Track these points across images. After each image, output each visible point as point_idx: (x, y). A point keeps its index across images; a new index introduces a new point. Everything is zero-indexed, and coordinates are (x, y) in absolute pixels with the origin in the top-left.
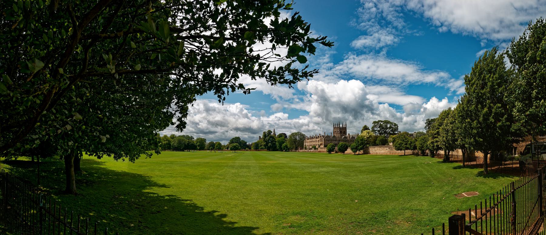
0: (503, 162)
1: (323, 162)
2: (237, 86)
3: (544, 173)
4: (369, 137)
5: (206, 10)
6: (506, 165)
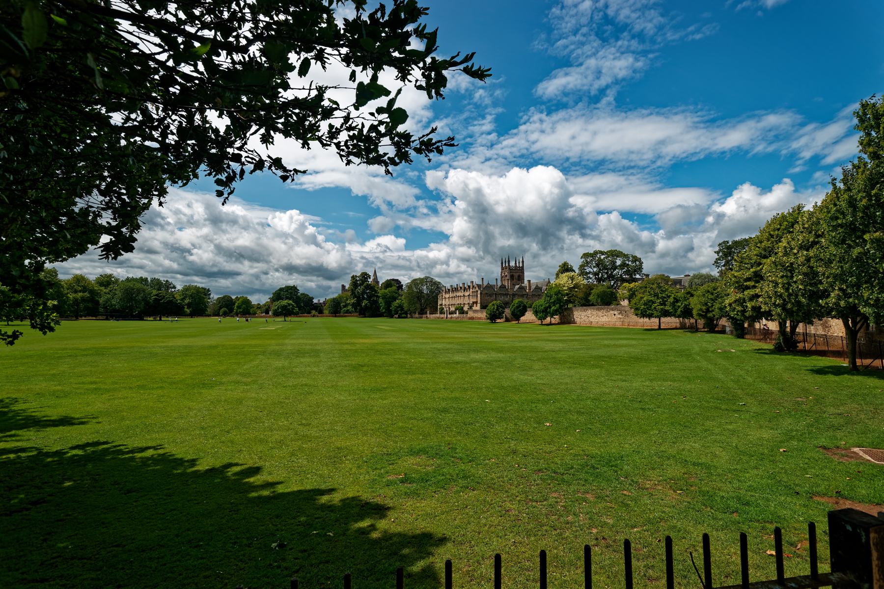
4: (574, 288)
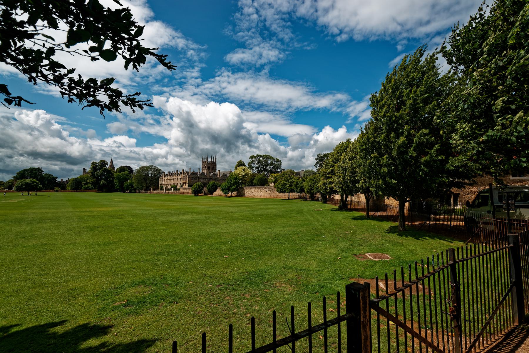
0: (432, 216)
1: (186, 207)
3: (525, 243)
4: (245, 175)
6: (438, 220)
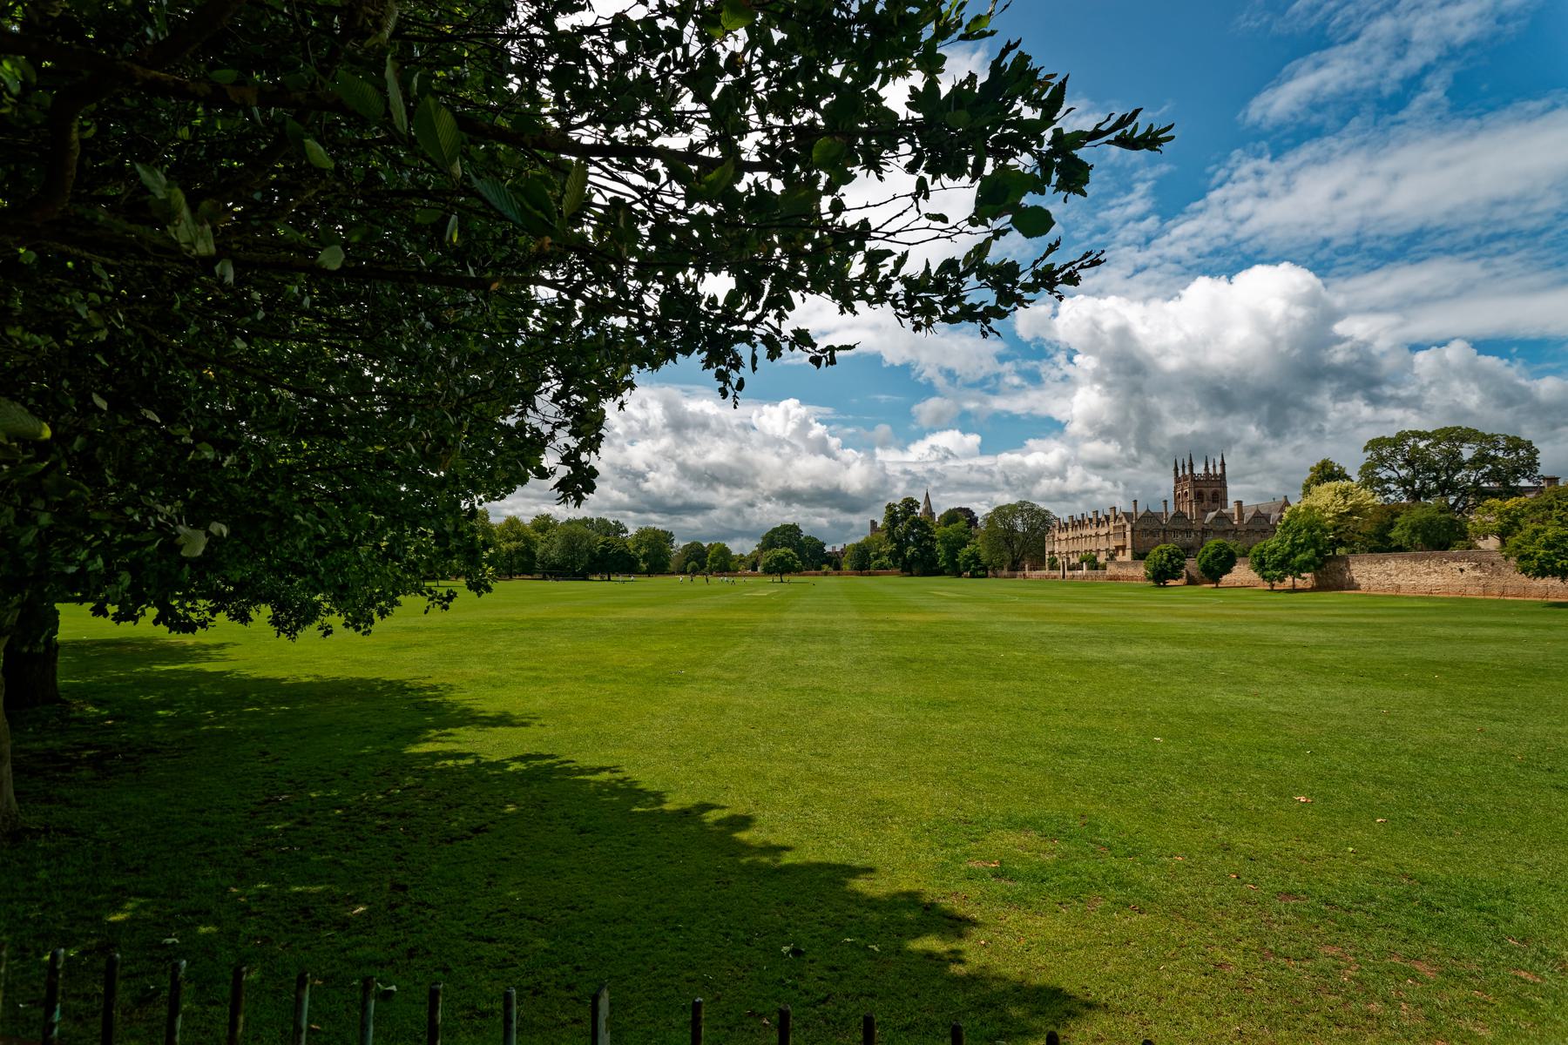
1: (1129, 619)
2: (786, 339)
5: (670, 54)
